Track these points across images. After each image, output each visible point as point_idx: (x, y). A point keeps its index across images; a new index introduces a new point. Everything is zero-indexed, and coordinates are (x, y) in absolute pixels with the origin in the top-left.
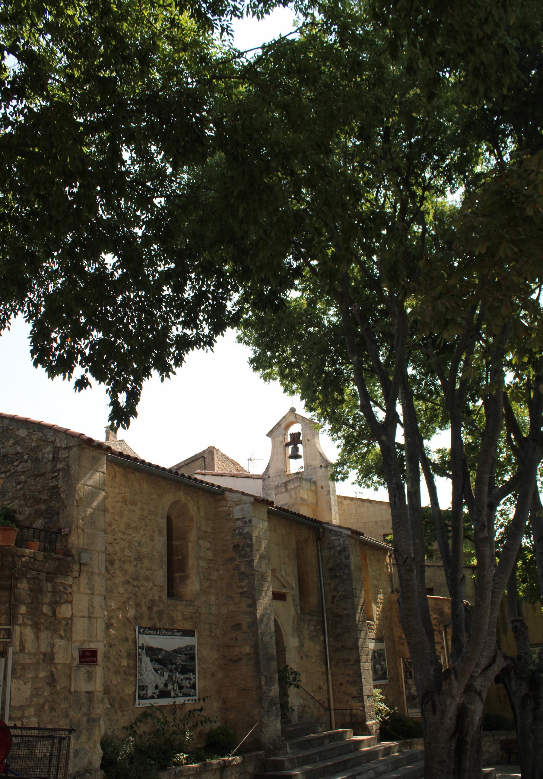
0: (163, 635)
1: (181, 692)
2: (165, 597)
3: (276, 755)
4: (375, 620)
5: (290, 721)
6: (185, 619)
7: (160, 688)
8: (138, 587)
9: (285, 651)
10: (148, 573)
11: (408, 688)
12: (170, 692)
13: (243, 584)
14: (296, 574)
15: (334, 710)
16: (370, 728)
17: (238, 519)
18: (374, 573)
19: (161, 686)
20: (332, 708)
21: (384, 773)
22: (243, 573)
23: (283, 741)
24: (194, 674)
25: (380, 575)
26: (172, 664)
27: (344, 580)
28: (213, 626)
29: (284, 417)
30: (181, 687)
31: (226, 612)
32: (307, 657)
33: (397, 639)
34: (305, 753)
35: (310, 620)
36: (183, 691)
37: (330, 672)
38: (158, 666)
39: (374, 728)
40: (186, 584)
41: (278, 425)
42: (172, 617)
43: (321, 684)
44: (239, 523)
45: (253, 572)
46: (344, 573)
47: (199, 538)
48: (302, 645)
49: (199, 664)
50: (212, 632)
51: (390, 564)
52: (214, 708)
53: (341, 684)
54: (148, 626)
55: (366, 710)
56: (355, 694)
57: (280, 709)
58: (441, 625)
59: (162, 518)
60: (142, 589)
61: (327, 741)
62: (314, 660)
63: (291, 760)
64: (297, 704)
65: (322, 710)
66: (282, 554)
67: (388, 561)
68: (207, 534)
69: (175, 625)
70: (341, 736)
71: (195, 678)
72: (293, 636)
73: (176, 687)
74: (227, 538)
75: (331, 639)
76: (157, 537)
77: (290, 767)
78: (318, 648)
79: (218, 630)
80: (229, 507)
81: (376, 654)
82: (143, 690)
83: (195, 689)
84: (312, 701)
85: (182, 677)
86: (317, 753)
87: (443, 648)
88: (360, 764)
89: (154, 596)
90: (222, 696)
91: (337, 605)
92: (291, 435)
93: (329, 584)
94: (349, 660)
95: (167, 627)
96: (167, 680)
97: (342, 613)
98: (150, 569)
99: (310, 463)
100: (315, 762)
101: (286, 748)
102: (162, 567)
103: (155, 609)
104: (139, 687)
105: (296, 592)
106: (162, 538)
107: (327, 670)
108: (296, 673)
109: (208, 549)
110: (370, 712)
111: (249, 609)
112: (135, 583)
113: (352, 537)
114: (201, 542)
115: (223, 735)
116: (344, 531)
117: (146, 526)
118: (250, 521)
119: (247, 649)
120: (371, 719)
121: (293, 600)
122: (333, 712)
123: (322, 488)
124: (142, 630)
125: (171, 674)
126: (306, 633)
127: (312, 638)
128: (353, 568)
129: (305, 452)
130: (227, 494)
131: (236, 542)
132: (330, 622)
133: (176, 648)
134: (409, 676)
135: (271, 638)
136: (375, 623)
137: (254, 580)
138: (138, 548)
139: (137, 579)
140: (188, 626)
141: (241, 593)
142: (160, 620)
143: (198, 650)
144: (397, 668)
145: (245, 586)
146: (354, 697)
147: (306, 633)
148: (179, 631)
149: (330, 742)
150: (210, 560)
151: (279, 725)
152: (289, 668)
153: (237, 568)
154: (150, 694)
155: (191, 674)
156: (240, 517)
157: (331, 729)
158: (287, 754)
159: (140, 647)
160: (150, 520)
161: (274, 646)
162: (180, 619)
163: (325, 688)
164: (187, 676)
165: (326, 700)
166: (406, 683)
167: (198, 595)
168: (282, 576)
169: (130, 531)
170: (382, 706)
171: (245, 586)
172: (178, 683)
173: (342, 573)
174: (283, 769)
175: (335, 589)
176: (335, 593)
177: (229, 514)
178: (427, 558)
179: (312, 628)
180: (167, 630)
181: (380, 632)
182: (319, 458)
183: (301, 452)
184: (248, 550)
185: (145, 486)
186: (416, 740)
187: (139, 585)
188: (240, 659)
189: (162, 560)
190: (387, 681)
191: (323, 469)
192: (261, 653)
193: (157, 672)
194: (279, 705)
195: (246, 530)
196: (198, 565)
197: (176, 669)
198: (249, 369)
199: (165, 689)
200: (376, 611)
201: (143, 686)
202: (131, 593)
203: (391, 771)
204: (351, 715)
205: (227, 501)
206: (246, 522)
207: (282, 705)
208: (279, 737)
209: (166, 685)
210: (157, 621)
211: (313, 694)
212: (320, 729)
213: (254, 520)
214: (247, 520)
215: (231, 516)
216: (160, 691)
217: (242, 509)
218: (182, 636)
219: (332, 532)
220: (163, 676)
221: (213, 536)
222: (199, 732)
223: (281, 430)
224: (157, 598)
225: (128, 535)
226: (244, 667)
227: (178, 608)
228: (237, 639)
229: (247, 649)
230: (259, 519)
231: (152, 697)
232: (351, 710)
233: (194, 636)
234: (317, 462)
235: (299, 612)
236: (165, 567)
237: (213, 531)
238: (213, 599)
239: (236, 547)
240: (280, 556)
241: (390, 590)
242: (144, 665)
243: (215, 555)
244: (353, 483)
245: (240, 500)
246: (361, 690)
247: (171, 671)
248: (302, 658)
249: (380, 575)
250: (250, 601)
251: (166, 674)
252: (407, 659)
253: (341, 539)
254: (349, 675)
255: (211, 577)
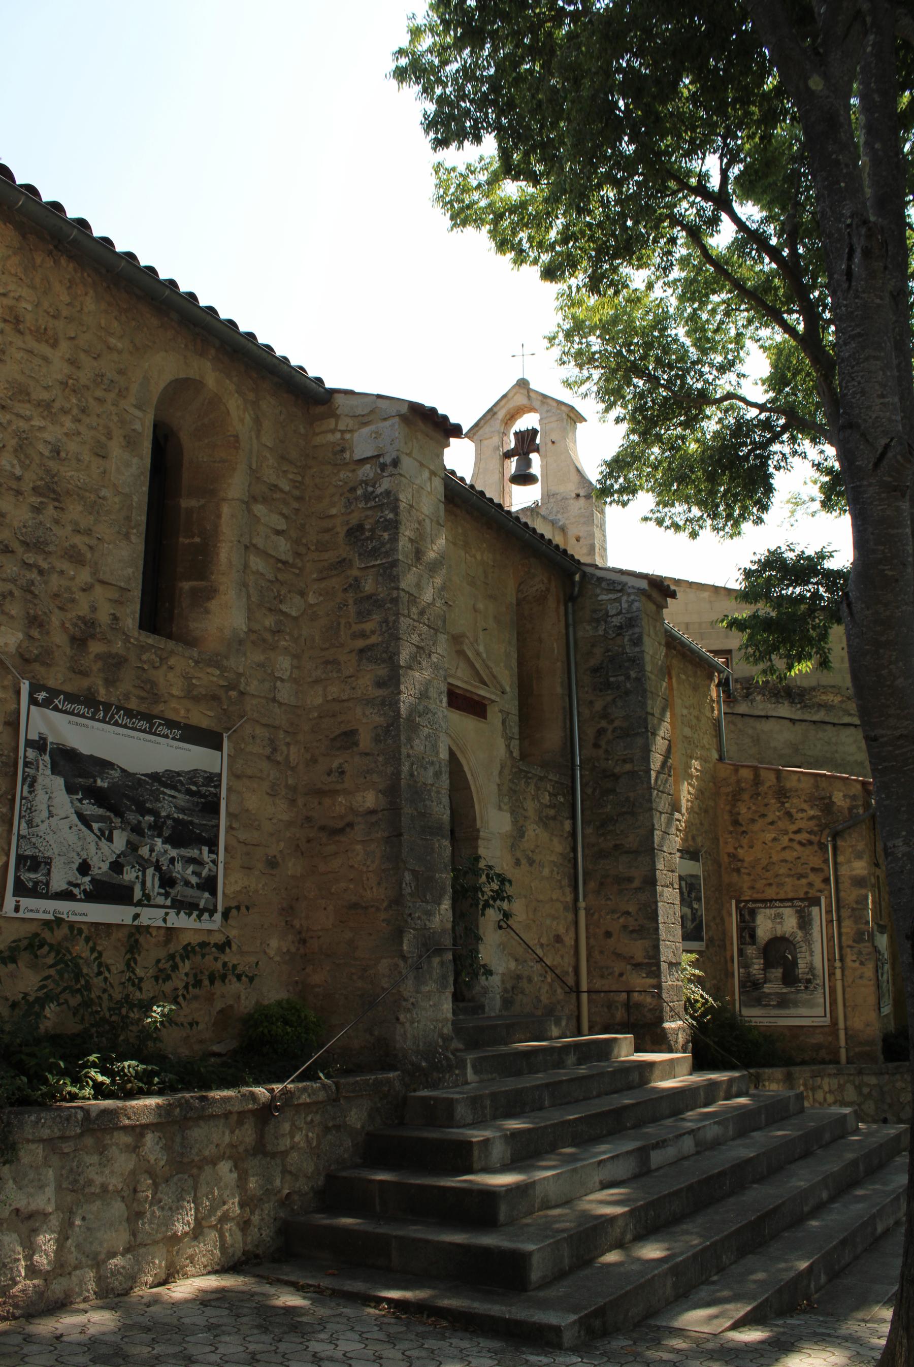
0: (116, 724)
1: (167, 895)
2: (130, 619)
3: (434, 1086)
4: (684, 810)
5: (482, 1007)
6: (191, 696)
7: (95, 871)
8: (41, 572)
9: (477, 838)
10: (79, 541)
11: (745, 964)
12: (130, 889)
13: (368, 626)
14: (514, 663)
15: (588, 992)
16: (672, 1038)
17: (363, 461)
18: (685, 712)
19: (101, 867)
20: (584, 986)
21: (716, 1144)
22: (369, 597)
23: (457, 1050)
24: (213, 850)
25: (698, 718)
26: (143, 810)
27: (627, 693)
28: (281, 735)
29: (504, 396)
30: (167, 882)
31: (319, 701)
32: (531, 862)
33: (725, 859)
34: (511, 1084)
35: (541, 779)
36: (173, 892)
37: (582, 904)
38: (90, 809)
39: (681, 1039)
40: (207, 612)
41: (491, 412)
42: (154, 684)
43: (561, 930)
44: (367, 471)
45: (395, 594)
46: (628, 677)
47: (255, 499)
48: (519, 832)
49: (230, 828)
50: (275, 750)
51: (718, 702)
52: (272, 953)
53: (608, 934)
54: (68, 688)
55: (664, 995)
56: (640, 957)
57: (451, 967)
58: (826, 832)
59: (139, 407)
60: (55, 581)
61: (571, 1059)
62: (546, 872)
63: (475, 1101)
64: (501, 970)
65: (559, 991)
66: (480, 606)
67: (714, 694)
68: (277, 495)
69: (161, 707)
70: (605, 1050)
71: (215, 862)
72: (500, 809)
73: (152, 878)
74: (334, 511)
75: (589, 831)
76: (116, 450)
77: (469, 1119)
78: (559, 846)
79: (293, 749)
80: (343, 432)
81: (683, 883)
82: (35, 867)
83: (214, 893)
84: (538, 967)
85: (173, 853)
86: (547, 1085)
87: (826, 880)
88: (655, 1120)
89: (94, 609)
90: (297, 923)
91: (606, 751)
92: (516, 434)
93: (591, 702)
94: (630, 880)
95: (133, 704)
96: (123, 854)
97: (617, 770)
98: (88, 532)
99: (554, 489)
100: (541, 1109)
101: (464, 1068)
102: (127, 536)
103: (96, 648)
104: (21, 859)
105: (512, 706)
106: (135, 460)
107: (576, 900)
108: (503, 880)
109: (278, 533)
110: (673, 1001)
111: (381, 692)
112: (30, 558)
113: (649, 597)
114: (259, 509)
115: (286, 1022)
116: (631, 581)
117: (83, 411)
118: (396, 463)
119: (369, 799)
120: (673, 1019)
121: (503, 722)
122: (584, 997)
123: (578, 540)
124: (42, 696)
125: (134, 837)
126: (531, 806)
127: (544, 821)
128: (648, 668)
129: (544, 468)
130: (339, 399)
131: (354, 519)
132: (589, 791)
133: (160, 769)
134: (748, 939)
135: (437, 774)
136: (682, 818)
137: (397, 614)
138: (51, 464)
139: (38, 546)
140: (202, 717)
141: (361, 651)
142: (110, 682)
143: (229, 789)
144: (722, 919)
145: (373, 632)
146: (637, 966)
147: (531, 806)
148: (171, 724)
149: (580, 1062)
150: (285, 563)
151: (447, 1006)
152: (482, 864)
153: (355, 585)
154: (58, 883)
155: (205, 849)
156: (369, 454)
157: (580, 1034)
158: (467, 1083)
159: (29, 743)
160: (101, 401)
161: (445, 800)
162: (175, 692)
163: (569, 940)
164: (193, 853)
165: (570, 969)
166: (741, 952)
167: (241, 642)
168: (478, 654)
169: (25, 409)
170: (697, 993)
171: (373, 632)
172: (158, 868)
173: (622, 678)
174: (450, 1121)
175: (605, 715)
176: (604, 724)
177: (343, 450)
178: (515, 1135)
179: (546, 799)
180: (129, 713)
181: (693, 838)
182: (575, 478)
183: (536, 468)
184: (386, 536)
185: (90, 304)
186: (768, 1071)
187: (45, 566)
188: (350, 825)
189: (128, 518)
190: (704, 943)
191: (582, 501)
192: (407, 810)
193: (90, 828)
194: (449, 956)
195: (385, 485)
196: (246, 566)
197: (157, 828)
198: (420, 131)
199: (116, 879)
200: (686, 793)
201: (34, 858)
202: (14, 581)
203: (733, 1139)
204: (628, 1005)
205: (337, 417)
206: (383, 467)
207: (457, 959)
208: (446, 1039)
209: (117, 867)
210: (100, 682)
211: (540, 952)
212: (555, 1032)
213: (407, 463)
214: (388, 459)
215: (347, 455)
216: (93, 881)
217: (377, 434)
218: (181, 740)
219: (604, 584)
220: (110, 839)
221: (296, 505)
222: (221, 1011)
223: (496, 424)
224: (103, 617)
225: (19, 416)
226: (359, 847)
227: (172, 661)
228: (343, 773)
229: (369, 799)
230: (422, 465)
231: (65, 895)
232: (629, 992)
233: (219, 748)
234: (571, 487)
235: (516, 754)
236: (138, 542)
237: (297, 493)
238: (284, 664)
239: (355, 532)
240: (475, 610)
241: (715, 755)
242: (41, 798)
243: (298, 554)
244: (646, 519)
245: (372, 412)
246: (656, 948)
247: (137, 829)
248: (518, 863)
249: (698, 718)
250: (382, 671)
251: (120, 840)
252: (747, 902)
253: (624, 598)
254: (628, 913)
255: (284, 608)
